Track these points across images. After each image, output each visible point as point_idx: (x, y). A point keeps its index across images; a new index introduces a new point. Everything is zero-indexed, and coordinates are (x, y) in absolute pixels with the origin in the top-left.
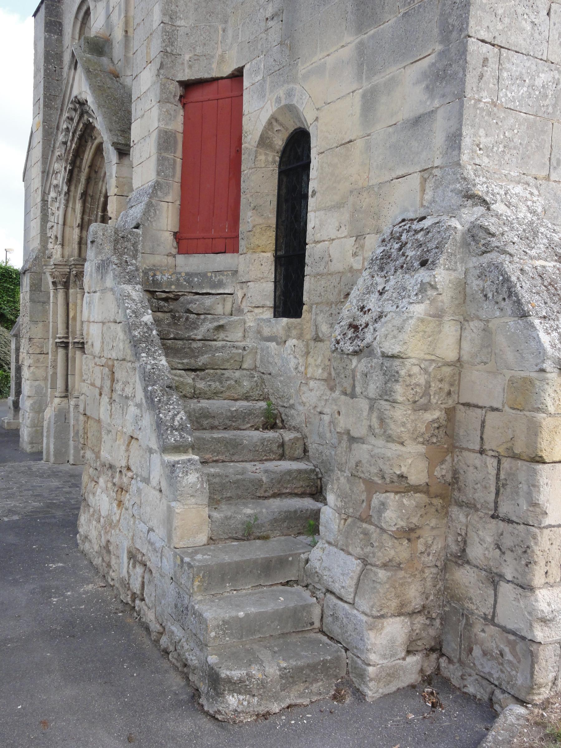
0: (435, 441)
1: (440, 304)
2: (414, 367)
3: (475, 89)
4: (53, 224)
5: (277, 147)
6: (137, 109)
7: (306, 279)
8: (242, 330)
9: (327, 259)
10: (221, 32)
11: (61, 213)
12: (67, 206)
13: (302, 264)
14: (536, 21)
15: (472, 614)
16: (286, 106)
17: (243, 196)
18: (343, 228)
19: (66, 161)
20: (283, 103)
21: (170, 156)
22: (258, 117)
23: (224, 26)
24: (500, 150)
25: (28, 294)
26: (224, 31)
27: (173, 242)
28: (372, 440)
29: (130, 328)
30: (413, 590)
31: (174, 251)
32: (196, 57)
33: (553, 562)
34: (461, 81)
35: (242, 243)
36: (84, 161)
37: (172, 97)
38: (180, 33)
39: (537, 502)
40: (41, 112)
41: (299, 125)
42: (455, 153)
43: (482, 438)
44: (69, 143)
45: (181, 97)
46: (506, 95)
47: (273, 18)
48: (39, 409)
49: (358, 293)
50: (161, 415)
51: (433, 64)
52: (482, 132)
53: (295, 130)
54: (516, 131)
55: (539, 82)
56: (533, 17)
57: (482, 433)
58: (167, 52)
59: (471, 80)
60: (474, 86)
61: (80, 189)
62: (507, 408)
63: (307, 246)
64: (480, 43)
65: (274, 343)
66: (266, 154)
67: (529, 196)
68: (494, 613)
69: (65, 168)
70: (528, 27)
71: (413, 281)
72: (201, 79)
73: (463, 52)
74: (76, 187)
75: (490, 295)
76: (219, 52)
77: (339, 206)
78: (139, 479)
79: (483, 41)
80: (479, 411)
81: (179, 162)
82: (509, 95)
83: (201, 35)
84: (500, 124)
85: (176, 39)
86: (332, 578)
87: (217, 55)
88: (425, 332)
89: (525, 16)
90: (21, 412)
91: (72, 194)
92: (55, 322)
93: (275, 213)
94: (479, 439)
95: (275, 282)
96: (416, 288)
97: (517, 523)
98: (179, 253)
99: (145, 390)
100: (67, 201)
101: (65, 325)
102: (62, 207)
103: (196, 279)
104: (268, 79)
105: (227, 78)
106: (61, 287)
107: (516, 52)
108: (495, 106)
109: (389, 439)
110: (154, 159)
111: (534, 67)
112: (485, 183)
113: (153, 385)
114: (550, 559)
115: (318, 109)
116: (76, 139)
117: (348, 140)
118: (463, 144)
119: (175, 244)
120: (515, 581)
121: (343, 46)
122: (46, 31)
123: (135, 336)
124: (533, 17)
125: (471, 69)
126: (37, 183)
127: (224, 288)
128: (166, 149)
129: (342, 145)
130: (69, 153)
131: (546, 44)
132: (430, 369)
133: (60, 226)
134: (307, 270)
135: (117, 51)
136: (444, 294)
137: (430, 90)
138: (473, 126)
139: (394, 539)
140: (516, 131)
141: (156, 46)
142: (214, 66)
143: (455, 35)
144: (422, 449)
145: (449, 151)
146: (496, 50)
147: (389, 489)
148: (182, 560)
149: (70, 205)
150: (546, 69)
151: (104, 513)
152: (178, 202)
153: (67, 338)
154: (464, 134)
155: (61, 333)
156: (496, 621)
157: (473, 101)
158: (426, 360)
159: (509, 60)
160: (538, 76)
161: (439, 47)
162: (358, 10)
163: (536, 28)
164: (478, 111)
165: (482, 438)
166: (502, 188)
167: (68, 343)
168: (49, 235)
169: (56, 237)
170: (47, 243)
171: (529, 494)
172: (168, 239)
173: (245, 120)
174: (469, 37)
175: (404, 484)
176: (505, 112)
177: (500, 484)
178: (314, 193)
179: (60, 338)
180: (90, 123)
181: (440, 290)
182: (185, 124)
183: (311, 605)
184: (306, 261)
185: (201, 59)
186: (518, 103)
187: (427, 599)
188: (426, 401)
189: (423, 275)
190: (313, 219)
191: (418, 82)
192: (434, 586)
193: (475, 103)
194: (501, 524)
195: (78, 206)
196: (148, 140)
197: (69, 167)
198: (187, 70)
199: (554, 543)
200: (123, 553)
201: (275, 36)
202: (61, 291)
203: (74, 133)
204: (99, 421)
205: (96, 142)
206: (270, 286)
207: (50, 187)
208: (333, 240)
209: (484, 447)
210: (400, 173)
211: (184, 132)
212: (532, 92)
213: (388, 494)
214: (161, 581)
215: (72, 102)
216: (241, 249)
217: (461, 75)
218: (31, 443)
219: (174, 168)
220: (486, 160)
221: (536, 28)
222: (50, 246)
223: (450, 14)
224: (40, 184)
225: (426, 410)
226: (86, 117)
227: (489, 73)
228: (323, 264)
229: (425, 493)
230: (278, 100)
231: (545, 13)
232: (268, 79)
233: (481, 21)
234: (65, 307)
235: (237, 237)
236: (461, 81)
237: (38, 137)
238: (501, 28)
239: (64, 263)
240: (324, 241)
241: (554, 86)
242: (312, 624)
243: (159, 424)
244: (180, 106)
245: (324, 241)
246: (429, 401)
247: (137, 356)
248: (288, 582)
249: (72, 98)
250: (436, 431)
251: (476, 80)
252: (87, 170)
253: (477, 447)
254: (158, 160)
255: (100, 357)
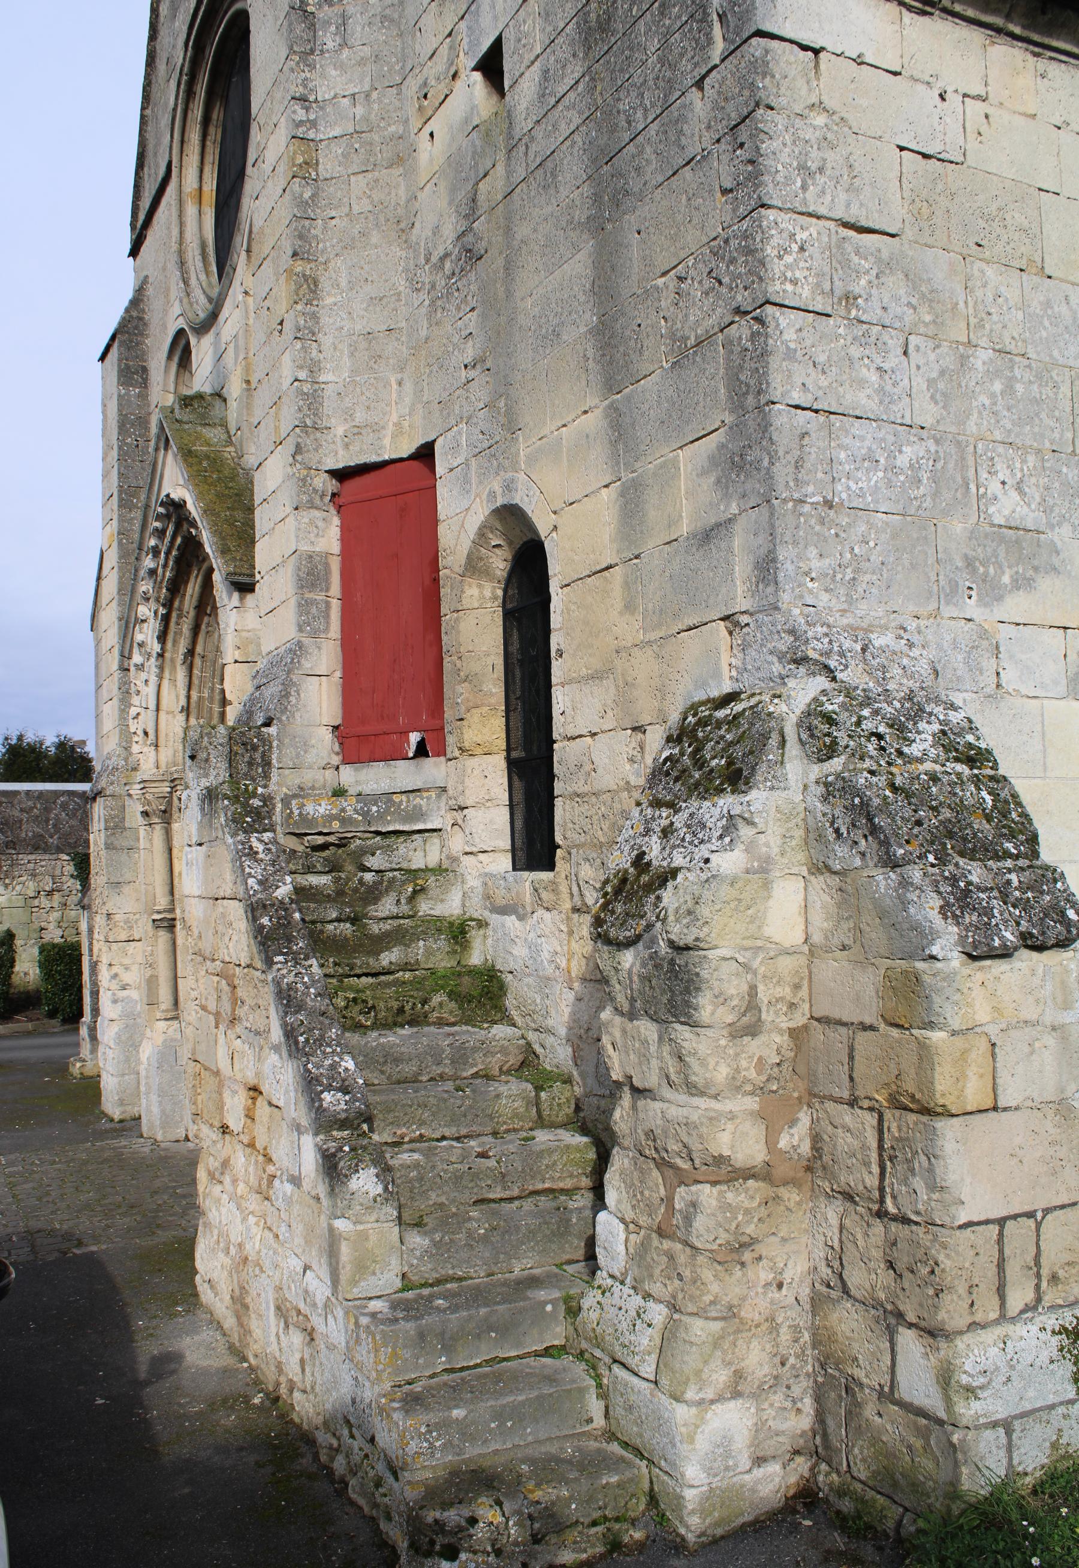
0: (774, 1088)
1: (764, 849)
2: (724, 964)
3: (792, 484)
4: (139, 710)
5: (499, 573)
6: (262, 519)
7: (558, 802)
8: (460, 894)
9: (588, 767)
10: (395, 386)
11: (151, 690)
12: (160, 677)
13: (550, 777)
14: (886, 366)
15: (861, 1385)
16: (504, 506)
17: (446, 660)
18: (610, 713)
19: (157, 600)
20: (500, 502)
21: (320, 597)
22: (463, 525)
23: (399, 376)
24: (847, 578)
25: (103, 835)
26: (400, 384)
27: (333, 743)
28: (667, 1092)
29: (254, 910)
30: (756, 1351)
31: (336, 760)
32: (356, 430)
33: (982, 1286)
34: (768, 473)
35: (450, 740)
36: (187, 597)
37: (318, 498)
38: (326, 393)
39: (944, 1184)
40: (115, 517)
41: (530, 536)
42: (770, 589)
43: (851, 1079)
44: (160, 571)
45: (334, 495)
46: (849, 488)
47: (474, 366)
48: (130, 1043)
49: (631, 832)
50: (310, 1066)
51: (722, 447)
52: (813, 552)
53: (525, 543)
54: (872, 544)
55: (902, 461)
56: (878, 361)
57: (851, 1069)
58: (306, 426)
59: (782, 472)
60: (790, 479)
61: (182, 648)
62: (882, 1026)
63: (555, 746)
64: (793, 410)
65: (513, 917)
66: (480, 586)
67: (905, 649)
68: (892, 1381)
69: (156, 613)
70: (874, 377)
71: (716, 812)
72: (365, 464)
73: (765, 427)
74: (175, 642)
75: (843, 830)
76: (394, 418)
77: (596, 676)
78: (285, 1178)
79: (797, 407)
80: (843, 1030)
81: (336, 606)
82: (853, 486)
83: (362, 394)
84: (843, 535)
85: (321, 404)
86: (784, 1240)
87: (391, 424)
88: (740, 900)
89: (866, 361)
90: (101, 1049)
91: (167, 655)
92: (11, 1049)
93: (502, 685)
94: (847, 1079)
95: (511, 806)
96: (720, 824)
97: (917, 1223)
98: (346, 761)
99: (284, 1025)
100: (161, 668)
101: (167, 888)
102: (153, 679)
103: (375, 809)
104: (473, 462)
105: (411, 458)
106: (157, 820)
107: (857, 417)
108: (831, 507)
109: (692, 1089)
110: (293, 602)
111: (891, 439)
112: (827, 635)
113: (297, 1012)
114: (976, 1281)
115: (555, 513)
116: (171, 563)
117: (604, 565)
118: (781, 575)
119: (337, 748)
120: (923, 1324)
121: (586, 412)
122: (119, 383)
123: (263, 927)
124: (878, 361)
125: (781, 453)
126: (111, 637)
127: (425, 822)
128: (313, 586)
129: (595, 574)
130: (161, 588)
131: (908, 399)
132: (755, 964)
133: (151, 714)
134: (558, 787)
135: (233, 412)
136: (770, 831)
137: (722, 484)
138: (795, 543)
139: (715, 1264)
140: (872, 544)
141: (288, 416)
142: (387, 441)
143: (750, 400)
144: (752, 1103)
145: (761, 586)
146: (821, 418)
147: (701, 1179)
148: (357, 1323)
149: (167, 674)
150: (912, 439)
151: (235, 1238)
152: (338, 674)
153: (172, 910)
154: (781, 558)
155: (162, 902)
156: (896, 1396)
157: (791, 504)
158: (746, 949)
159: (847, 431)
160: (900, 452)
161: (729, 419)
162: (603, 355)
163: (887, 377)
164: (802, 520)
165: (851, 1079)
166: (856, 642)
167: (174, 919)
168: (132, 730)
169: (146, 734)
170: (130, 742)
171: (931, 1170)
172: (324, 744)
173: (442, 529)
174: (773, 403)
175: (725, 1169)
176: (849, 515)
177: (885, 1155)
178: (560, 653)
179: (159, 912)
180: (194, 537)
181: (761, 826)
182: (344, 540)
183: (587, 1388)
184: (556, 771)
185: (363, 431)
186: (870, 499)
187: (783, 1364)
188: (754, 1019)
189: (727, 802)
190: (560, 698)
191: (704, 473)
192: (796, 1341)
193: (795, 506)
194: (894, 1227)
195: (181, 674)
196: (281, 570)
197: (162, 611)
198: (341, 452)
199: (982, 1252)
200: (268, 1308)
201: (480, 393)
202: (158, 827)
203: (168, 553)
204: (217, 1073)
205: (205, 566)
206: (504, 814)
207: (131, 647)
208: (595, 734)
209: (857, 1093)
210: (691, 622)
211: (346, 553)
212: (894, 478)
213: (699, 1186)
214: (329, 1359)
215: (162, 504)
216: (449, 750)
217: (766, 463)
218: (121, 1102)
219: (327, 616)
220: (825, 597)
221: (887, 377)
222: (135, 749)
223: (741, 367)
224: (116, 640)
225: (754, 1035)
226: (185, 526)
227: (814, 456)
228: (581, 776)
229: (764, 1179)
230: (492, 495)
231: (900, 351)
232: (473, 462)
233: (789, 377)
234: (166, 855)
235: (443, 728)
236: (768, 473)
237: (112, 558)
238: (826, 383)
239: (160, 778)
240: (580, 736)
241: (931, 463)
242: (590, 1420)
243: (311, 1085)
244: (333, 511)
245: (580, 736)
246: (760, 1019)
247: (269, 963)
248: (547, 1349)
249: (163, 493)
250: (776, 1070)
251: (791, 469)
252: (192, 613)
253: (846, 1094)
254: (300, 605)
255: (214, 960)
